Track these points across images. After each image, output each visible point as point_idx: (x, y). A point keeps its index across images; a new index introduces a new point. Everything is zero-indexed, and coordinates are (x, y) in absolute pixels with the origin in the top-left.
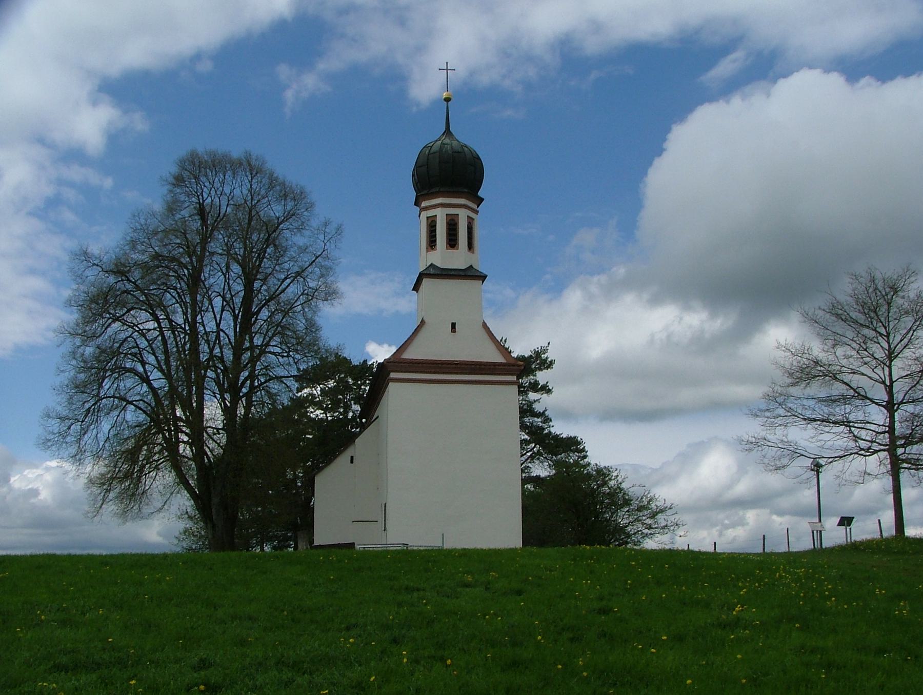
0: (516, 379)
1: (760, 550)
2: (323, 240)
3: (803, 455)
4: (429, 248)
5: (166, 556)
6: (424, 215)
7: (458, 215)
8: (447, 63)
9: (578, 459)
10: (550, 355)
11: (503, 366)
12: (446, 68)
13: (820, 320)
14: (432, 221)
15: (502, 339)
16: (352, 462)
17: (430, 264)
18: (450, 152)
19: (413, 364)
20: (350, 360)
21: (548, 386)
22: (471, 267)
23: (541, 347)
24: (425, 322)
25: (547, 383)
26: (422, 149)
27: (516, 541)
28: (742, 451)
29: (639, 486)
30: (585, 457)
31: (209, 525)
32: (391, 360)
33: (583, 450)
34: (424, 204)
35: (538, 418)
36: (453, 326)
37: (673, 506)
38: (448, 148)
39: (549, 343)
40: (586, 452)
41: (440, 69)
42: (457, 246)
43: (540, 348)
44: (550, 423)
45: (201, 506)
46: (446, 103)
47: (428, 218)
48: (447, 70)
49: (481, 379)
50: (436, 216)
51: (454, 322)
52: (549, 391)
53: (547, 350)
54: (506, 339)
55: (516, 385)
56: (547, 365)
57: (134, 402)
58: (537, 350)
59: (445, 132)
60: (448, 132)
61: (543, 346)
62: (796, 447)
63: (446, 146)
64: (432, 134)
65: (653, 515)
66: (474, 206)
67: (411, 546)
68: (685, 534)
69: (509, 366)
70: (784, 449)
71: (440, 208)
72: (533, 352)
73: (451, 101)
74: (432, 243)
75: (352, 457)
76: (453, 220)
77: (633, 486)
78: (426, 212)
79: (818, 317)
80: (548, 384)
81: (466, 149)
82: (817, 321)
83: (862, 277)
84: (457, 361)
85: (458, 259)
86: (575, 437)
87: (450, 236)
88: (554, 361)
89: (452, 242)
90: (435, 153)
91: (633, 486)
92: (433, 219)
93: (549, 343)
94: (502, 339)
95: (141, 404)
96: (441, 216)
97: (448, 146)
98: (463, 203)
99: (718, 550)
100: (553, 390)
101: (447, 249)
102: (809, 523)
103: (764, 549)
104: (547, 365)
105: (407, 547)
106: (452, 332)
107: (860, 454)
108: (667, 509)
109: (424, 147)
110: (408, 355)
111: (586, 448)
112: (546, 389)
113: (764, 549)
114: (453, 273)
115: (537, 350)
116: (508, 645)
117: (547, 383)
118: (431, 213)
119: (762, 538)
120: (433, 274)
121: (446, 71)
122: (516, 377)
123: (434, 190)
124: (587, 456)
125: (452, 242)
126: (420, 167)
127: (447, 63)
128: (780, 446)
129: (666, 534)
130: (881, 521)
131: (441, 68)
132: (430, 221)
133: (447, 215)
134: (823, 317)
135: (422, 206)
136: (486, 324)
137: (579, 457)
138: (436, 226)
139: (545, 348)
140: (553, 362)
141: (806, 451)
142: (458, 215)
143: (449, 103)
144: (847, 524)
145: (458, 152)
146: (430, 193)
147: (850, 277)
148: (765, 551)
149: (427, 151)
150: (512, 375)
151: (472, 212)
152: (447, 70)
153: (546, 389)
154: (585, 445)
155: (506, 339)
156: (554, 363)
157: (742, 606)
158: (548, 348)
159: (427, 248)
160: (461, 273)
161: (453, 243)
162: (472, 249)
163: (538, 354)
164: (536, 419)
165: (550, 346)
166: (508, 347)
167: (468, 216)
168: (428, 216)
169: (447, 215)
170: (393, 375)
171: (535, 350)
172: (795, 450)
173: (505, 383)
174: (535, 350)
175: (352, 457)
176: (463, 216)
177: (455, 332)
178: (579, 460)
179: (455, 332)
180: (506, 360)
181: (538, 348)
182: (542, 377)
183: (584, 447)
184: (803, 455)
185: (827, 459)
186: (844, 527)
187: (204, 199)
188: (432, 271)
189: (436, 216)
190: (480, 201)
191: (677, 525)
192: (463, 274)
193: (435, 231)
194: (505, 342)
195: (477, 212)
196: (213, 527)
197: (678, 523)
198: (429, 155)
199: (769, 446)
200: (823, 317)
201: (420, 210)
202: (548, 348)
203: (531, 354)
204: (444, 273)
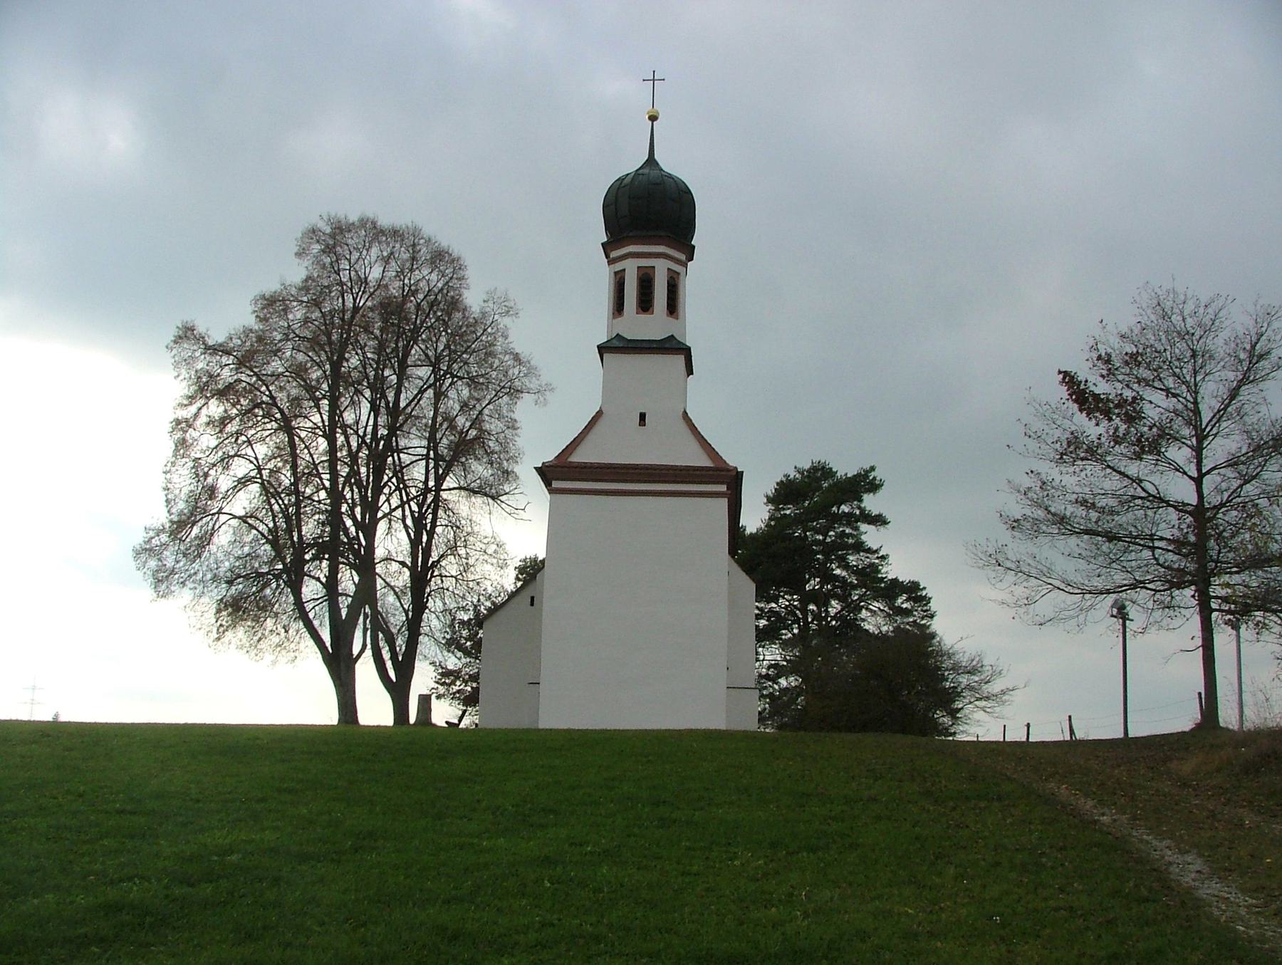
0: (725, 489)
4: (616, 313)
7: (654, 267)
10: (878, 474)
11: (713, 471)
14: (620, 278)
16: (532, 604)
17: (615, 335)
19: (601, 468)
24: (603, 413)
34: (614, 254)
36: (643, 417)
41: (644, 80)
48: (654, 80)
50: (624, 270)
55: (725, 497)
56: (874, 487)
60: (651, 161)
63: (641, 176)
64: (632, 162)
66: (683, 257)
73: (658, 121)
74: (618, 307)
75: (532, 598)
85: (653, 326)
86: (896, 579)
89: (645, 304)
96: (631, 268)
98: (661, 251)
99: (1007, 740)
101: (653, 313)
106: (640, 425)
112: (879, 520)
114: (644, 345)
116: (1098, 805)
121: (652, 82)
122: (726, 486)
125: (645, 304)
130: (1072, 717)
131: (645, 79)
132: (618, 276)
133: (638, 267)
142: (654, 267)
143: (655, 123)
150: (722, 483)
151: (675, 263)
153: (879, 520)
159: (613, 314)
162: (675, 314)
167: (668, 269)
168: (616, 270)
169: (638, 267)
173: (696, 495)
175: (532, 598)
176: (661, 269)
177: (645, 425)
179: (645, 425)
180: (713, 462)
182: (870, 503)
189: (624, 270)
190: (690, 252)
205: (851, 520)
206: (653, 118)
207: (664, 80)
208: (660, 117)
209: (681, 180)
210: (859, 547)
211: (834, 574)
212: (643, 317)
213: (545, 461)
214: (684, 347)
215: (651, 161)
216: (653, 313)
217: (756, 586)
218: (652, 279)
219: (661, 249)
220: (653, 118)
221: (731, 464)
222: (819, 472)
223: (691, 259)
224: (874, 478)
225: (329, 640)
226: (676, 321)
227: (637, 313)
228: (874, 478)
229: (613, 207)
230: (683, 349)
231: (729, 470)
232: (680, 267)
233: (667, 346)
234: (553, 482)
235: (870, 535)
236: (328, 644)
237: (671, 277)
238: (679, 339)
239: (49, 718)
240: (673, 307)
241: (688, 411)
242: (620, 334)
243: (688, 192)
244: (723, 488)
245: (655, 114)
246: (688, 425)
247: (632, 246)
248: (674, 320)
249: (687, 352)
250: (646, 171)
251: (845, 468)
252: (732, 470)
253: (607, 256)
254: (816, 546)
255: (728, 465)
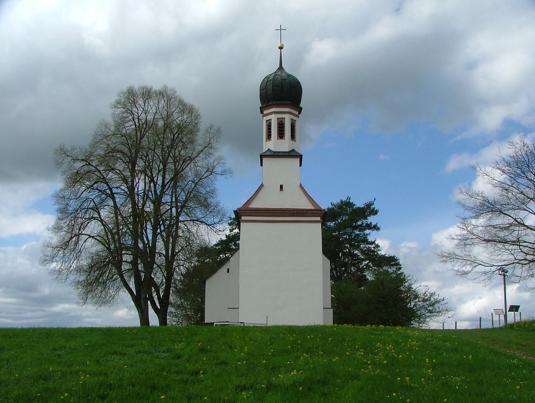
1: (491, 327)
2: (209, 137)
3: (480, 264)
4: (267, 139)
5: (34, 330)
6: (266, 118)
7: (285, 118)
8: (281, 26)
9: (396, 270)
10: (376, 206)
12: (280, 29)
13: (490, 173)
15: (348, 197)
16: (228, 272)
17: (267, 149)
18: (279, 80)
20: (370, 217)
21: (377, 226)
22: (293, 150)
23: (370, 202)
25: (377, 223)
26: (264, 79)
27: (139, 325)
28: (441, 262)
29: (424, 286)
30: (400, 268)
31: (139, 310)
32: (241, 209)
33: (398, 264)
34: (265, 112)
35: (372, 245)
36: (281, 187)
37: (444, 299)
38: (279, 77)
39: (375, 199)
40: (400, 265)
42: (284, 137)
43: (369, 202)
44: (379, 248)
45: (135, 299)
46: (280, 50)
47: (267, 121)
49: (277, 220)
50: (271, 119)
51: (282, 184)
52: (378, 229)
53: (374, 203)
54: (350, 198)
56: (375, 212)
57: (95, 237)
58: (367, 203)
59: (279, 68)
60: (281, 68)
61: (371, 201)
62: (475, 259)
63: (277, 76)
65: (433, 305)
66: (297, 113)
67: (246, 324)
68: (452, 316)
69: (315, 211)
70: (467, 260)
71: (273, 115)
72: (365, 205)
74: (269, 136)
75: (228, 269)
76: (282, 121)
77: (420, 286)
78: (265, 117)
79: (488, 172)
80: (377, 225)
81: (290, 77)
82: (487, 174)
83: (518, 144)
84: (283, 209)
85: (285, 145)
87: (279, 131)
88: (378, 210)
89: (281, 135)
90: (270, 81)
91: (420, 286)
92: (270, 121)
93: (375, 199)
94: (348, 197)
95: (98, 238)
96: (274, 119)
97: (279, 76)
100: (381, 228)
101: (285, 139)
102: (494, 309)
103: (480, 326)
104: (375, 212)
105: (244, 324)
106: (280, 191)
107: (520, 264)
108: (441, 301)
109: (265, 78)
110: (255, 205)
111: (400, 263)
112: (376, 228)
113: (480, 326)
114: (282, 154)
115: (367, 203)
117: (377, 223)
118: (268, 118)
119: (479, 319)
120: (269, 155)
121: (280, 31)
122: (320, 218)
123: (271, 103)
124: (401, 268)
125: (281, 135)
126: (262, 90)
127: (281, 26)
128: (465, 259)
129: (441, 316)
132: (268, 122)
133: (277, 118)
134: (491, 172)
135: (264, 113)
136: (302, 185)
137: (397, 269)
138: (271, 126)
139: (372, 202)
140: (377, 211)
141: (482, 262)
142: (285, 118)
143: (282, 50)
144: (515, 310)
145: (285, 79)
146: (268, 105)
147: (509, 144)
148: (481, 327)
149: (266, 80)
152: (281, 30)
154: (399, 261)
155: (350, 198)
156: (378, 212)
157: (298, 371)
158: (374, 202)
159: (266, 140)
160: (286, 154)
161: (282, 136)
162: (294, 139)
163: (369, 205)
164: (370, 246)
165: (375, 201)
166: (352, 202)
167: (291, 119)
168: (267, 119)
169: (277, 118)
170: (243, 218)
171: (366, 203)
172: (474, 261)
174: (366, 203)
175: (228, 269)
176: (288, 119)
177: (283, 190)
178: (397, 270)
181: (368, 202)
182: (372, 220)
183: (399, 262)
184: (480, 264)
185: (497, 267)
186: (513, 312)
187: (139, 116)
188: (268, 153)
189: (271, 119)
190: (300, 110)
191: (447, 310)
192: (288, 155)
193: (271, 129)
194: (350, 199)
195: (298, 116)
196: (141, 311)
197: (448, 308)
198: (267, 82)
199: (457, 259)
200: (491, 172)
201: (263, 116)
202: (374, 202)
203: (364, 206)
204: (275, 154)
205: (362, 228)
206: (281, 48)
207: (285, 30)
208: (284, 48)
209: (296, 78)
210: (365, 241)
211: (111, 193)
212: (280, 141)
213: (238, 208)
214: (299, 155)
215: (281, 68)
216: (285, 139)
217: (330, 262)
218: (284, 123)
219: (287, 110)
220: (281, 48)
221: (322, 208)
222: (347, 204)
223: (300, 113)
224: (374, 208)
225: (509, 308)
226: (295, 142)
227: (277, 139)
228: (374, 208)
229: (265, 90)
230: (299, 155)
231: (321, 210)
232: (296, 118)
233: (292, 154)
234: (242, 217)
235: (372, 235)
236: (135, 293)
237: (292, 122)
238: (297, 151)
239: (128, 326)
240: (293, 137)
241: (301, 184)
242: (270, 149)
243: (298, 83)
244: (319, 219)
245: (282, 46)
246: (302, 190)
247: (274, 108)
248: (294, 142)
249: (300, 157)
250: (279, 73)
251: (359, 203)
252: (323, 211)
253: (262, 112)
254: (340, 239)
255: (321, 208)
